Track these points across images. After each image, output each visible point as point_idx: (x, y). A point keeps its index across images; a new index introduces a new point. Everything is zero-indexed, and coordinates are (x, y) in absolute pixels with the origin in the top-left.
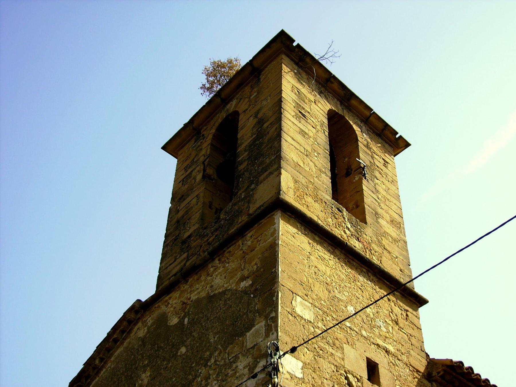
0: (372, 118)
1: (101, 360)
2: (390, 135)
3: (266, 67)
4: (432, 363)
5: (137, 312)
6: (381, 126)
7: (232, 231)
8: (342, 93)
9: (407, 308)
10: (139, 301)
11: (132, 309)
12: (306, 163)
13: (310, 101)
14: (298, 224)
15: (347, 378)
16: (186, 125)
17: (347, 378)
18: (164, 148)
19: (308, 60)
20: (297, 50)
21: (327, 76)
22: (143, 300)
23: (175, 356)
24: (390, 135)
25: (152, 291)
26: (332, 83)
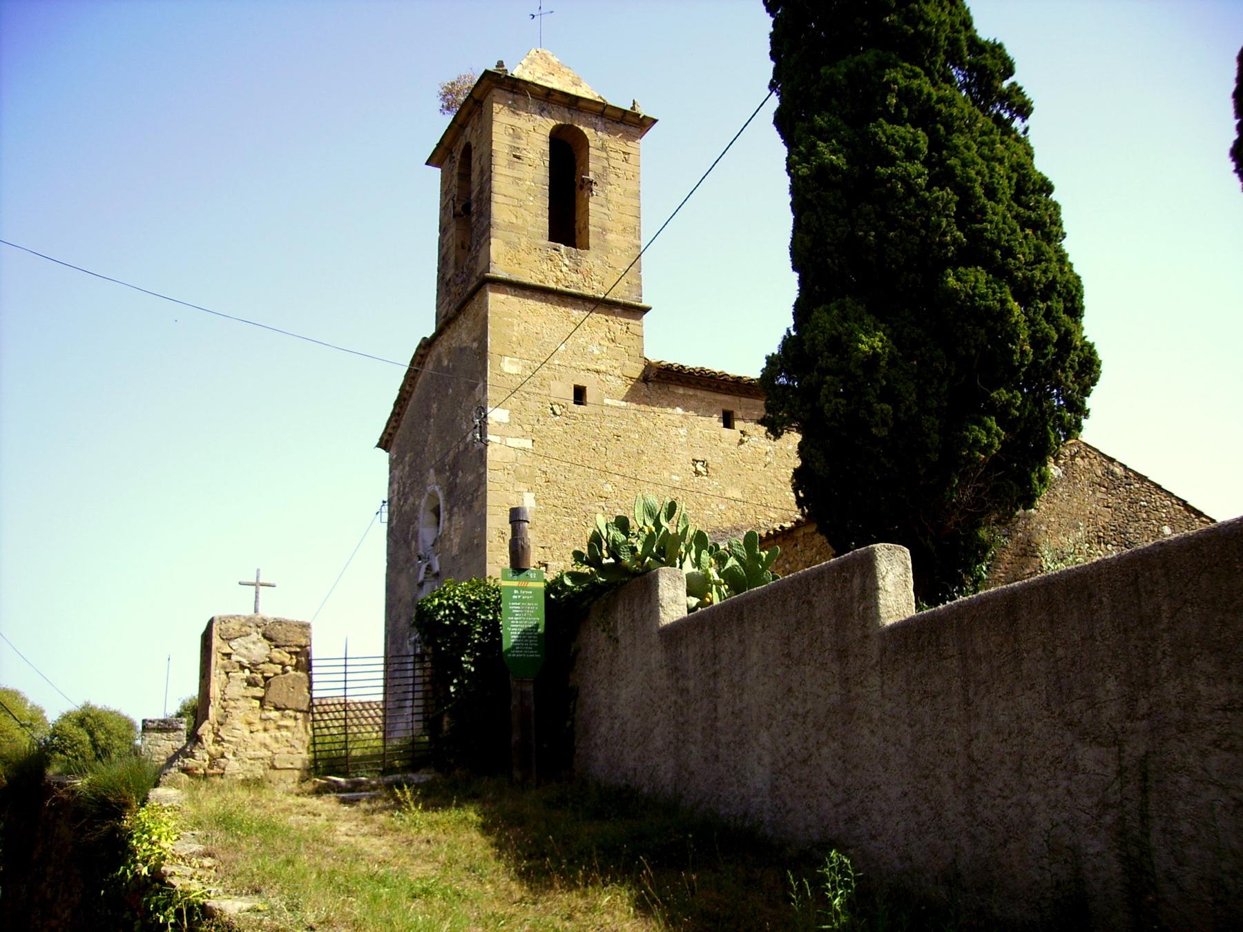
0: (607, 111)
1: (410, 385)
2: (633, 119)
3: (485, 98)
4: (649, 366)
5: (424, 348)
6: (619, 114)
7: (469, 289)
8: (567, 100)
9: (627, 321)
10: (425, 338)
11: (420, 346)
12: (519, 215)
13: (528, 132)
14: (508, 289)
15: (552, 409)
16: (438, 145)
17: (552, 409)
18: (427, 163)
19: (521, 85)
20: (506, 80)
21: (545, 91)
22: (428, 336)
23: (447, 394)
24: (633, 119)
25: (433, 331)
26: (553, 95)
